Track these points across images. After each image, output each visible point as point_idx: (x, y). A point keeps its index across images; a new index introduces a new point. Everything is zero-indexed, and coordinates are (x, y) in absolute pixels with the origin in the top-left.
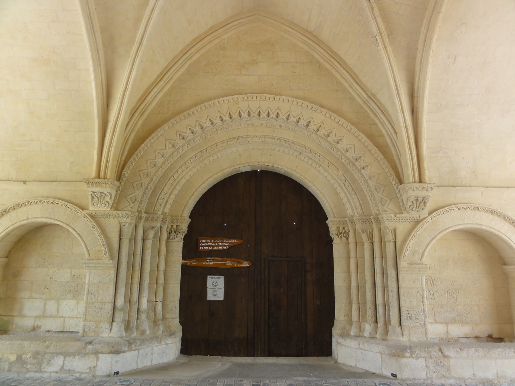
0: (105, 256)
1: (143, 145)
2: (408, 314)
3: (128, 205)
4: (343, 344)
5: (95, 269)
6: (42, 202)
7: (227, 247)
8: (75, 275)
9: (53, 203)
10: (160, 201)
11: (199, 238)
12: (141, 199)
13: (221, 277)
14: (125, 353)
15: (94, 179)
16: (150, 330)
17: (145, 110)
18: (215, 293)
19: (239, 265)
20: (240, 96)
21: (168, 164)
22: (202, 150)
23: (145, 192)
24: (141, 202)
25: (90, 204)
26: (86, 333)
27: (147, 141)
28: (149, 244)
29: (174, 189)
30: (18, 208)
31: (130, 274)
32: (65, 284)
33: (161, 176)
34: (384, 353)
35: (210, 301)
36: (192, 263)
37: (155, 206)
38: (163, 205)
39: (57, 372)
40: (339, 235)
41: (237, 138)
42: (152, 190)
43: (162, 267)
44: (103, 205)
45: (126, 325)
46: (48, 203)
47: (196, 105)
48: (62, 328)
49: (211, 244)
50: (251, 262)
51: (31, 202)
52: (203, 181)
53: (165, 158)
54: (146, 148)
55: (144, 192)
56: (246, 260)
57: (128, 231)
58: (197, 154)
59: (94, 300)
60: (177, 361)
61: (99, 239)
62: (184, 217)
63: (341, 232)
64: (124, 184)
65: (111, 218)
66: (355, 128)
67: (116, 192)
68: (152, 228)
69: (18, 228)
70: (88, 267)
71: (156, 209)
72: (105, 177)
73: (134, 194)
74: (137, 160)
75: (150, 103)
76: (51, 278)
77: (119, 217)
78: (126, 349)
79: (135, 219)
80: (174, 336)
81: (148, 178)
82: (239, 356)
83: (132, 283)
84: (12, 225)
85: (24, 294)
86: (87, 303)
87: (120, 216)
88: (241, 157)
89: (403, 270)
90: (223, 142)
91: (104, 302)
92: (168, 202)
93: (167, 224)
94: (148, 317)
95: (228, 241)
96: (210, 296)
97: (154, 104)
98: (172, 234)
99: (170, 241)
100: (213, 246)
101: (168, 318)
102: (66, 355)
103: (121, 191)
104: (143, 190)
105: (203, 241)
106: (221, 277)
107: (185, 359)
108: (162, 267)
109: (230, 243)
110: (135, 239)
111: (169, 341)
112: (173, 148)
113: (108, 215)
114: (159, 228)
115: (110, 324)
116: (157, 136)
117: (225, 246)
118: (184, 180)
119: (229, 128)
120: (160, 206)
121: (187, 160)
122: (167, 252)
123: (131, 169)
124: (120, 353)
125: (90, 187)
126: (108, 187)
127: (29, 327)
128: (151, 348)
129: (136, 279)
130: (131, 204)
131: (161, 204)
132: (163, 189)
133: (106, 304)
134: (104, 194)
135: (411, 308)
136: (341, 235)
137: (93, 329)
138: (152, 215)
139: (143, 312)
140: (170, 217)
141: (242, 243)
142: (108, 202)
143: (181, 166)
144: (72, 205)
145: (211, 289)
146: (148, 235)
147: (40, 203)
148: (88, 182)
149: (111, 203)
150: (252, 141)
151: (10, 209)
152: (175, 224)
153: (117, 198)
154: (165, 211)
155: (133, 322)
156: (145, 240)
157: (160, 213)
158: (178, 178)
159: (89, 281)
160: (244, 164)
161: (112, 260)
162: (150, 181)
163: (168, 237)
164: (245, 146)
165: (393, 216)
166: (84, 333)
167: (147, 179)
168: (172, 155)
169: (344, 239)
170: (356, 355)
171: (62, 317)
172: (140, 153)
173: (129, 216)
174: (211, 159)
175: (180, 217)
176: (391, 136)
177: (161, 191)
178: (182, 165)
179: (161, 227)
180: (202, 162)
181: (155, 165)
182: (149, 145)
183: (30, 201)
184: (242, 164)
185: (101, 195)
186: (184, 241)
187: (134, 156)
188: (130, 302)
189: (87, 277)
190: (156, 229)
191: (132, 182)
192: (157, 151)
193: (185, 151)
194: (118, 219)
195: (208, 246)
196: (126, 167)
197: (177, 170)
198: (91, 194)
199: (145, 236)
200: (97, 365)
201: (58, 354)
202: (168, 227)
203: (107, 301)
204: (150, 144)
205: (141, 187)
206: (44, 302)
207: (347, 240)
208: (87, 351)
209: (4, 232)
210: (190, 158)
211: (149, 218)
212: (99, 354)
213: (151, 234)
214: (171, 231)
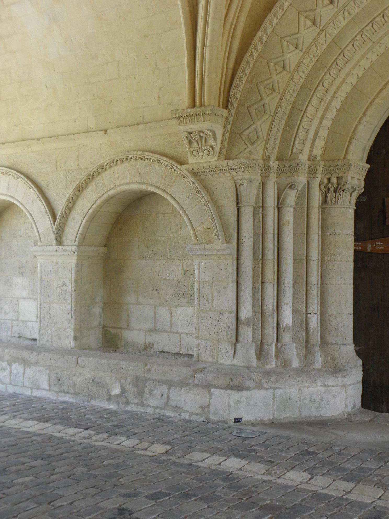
1: (259, 33)
5: (206, 259)
6: (129, 158)
8: (188, 270)
9: (142, 159)
11: (386, 199)
12: (268, 135)
14: (250, 390)
16: (300, 360)
21: (310, 62)
22: (374, 19)
23: (274, 121)
24: (268, 140)
25: (189, 154)
27: (266, 23)
30: (103, 172)
31: (258, 266)
32: (176, 284)
33: (300, 86)
36: (374, 247)
37: (293, 146)
38: (308, 143)
39: (161, 408)
43: (314, 255)
46: (136, 160)
48: (179, 349)
51: (115, 160)
53: (304, 51)
54: (264, 39)
55: (271, 122)
58: (364, 28)
59: (207, 307)
65: (221, 175)
67: (225, 127)
68: (292, 186)
69: (108, 201)
71: (295, 150)
72: (202, 105)
73: (252, 128)
74: (254, 65)
76: (158, 276)
77: (232, 170)
78: (252, 385)
81: (275, 94)
84: (99, 198)
85: (130, 298)
92: (318, 135)
98: (330, 194)
99: (327, 208)
101: (331, 344)
102: (170, 384)
107: (368, 415)
108: (314, 255)
110: (263, 207)
112: (314, 27)
113: (217, 169)
114: (305, 185)
115: (231, 346)
116: (283, 9)
118: (347, 88)
120: (303, 144)
121: (345, 46)
123: (244, 82)
124: (242, 390)
125: (182, 125)
126: (207, 120)
127: (139, 344)
128: (297, 390)
129: (270, 274)
130: (249, 145)
132: (305, 112)
133: (224, 314)
138: (287, 162)
140: (322, 163)
142: (212, 147)
143: (335, 61)
144: (165, 159)
146: (284, 198)
147: (127, 161)
148: (179, 117)
149: (218, 147)
151: (93, 174)
152: (334, 175)
154: (314, 153)
156: (281, 207)
157: (304, 157)
158: (331, 85)
159: (199, 278)
161: (227, 243)
163: (325, 201)
167: (272, 96)
168: (315, 42)
171: (177, 332)
172: (255, 49)
173: (246, 167)
177: (303, 116)
178: (336, 59)
179: (308, 182)
180: (378, 43)
181: (284, 68)
183: (114, 159)
185: (200, 136)
187: (247, 57)
190: (300, 187)
191: (247, 106)
194: (231, 175)
196: (236, 79)
197: (329, 69)
199: (281, 200)
200: (210, 404)
201: (162, 382)
202: (323, 183)
203: (225, 309)
204: (272, 29)
205: (265, 112)
206: (154, 309)
208: (196, 382)
209: (92, 208)
210: (350, 40)
212: (212, 388)
214: (329, 189)
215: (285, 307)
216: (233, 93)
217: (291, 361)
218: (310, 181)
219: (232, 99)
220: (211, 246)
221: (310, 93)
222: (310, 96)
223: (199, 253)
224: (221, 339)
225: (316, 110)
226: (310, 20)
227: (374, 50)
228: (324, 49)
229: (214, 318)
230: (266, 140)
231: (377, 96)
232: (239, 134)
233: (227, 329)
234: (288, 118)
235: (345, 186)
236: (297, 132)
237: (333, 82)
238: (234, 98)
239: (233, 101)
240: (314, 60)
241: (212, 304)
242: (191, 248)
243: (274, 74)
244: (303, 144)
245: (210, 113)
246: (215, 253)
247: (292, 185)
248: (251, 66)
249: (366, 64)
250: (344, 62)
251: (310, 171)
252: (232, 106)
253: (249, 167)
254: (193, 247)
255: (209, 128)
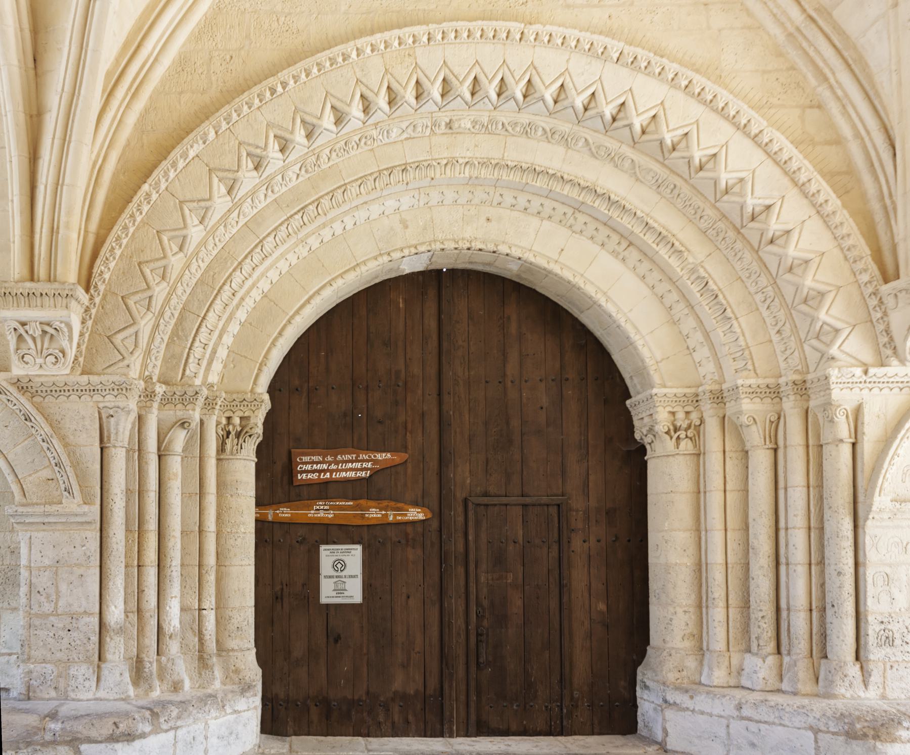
0: (66, 493)
1: (146, 187)
2: (882, 632)
3: (118, 359)
4: (684, 706)
5: (44, 530)
7: (366, 473)
10: (198, 351)
13: (354, 549)
15: (20, 284)
16: (191, 679)
17: (141, 83)
18: (339, 587)
19: (400, 518)
20: (421, 30)
22: (306, 206)
23: (158, 325)
26: (34, 692)
27: (158, 173)
28: (175, 465)
29: (231, 319)
33: (196, 280)
34: (825, 729)
35: (327, 605)
36: (278, 514)
38: (204, 363)
40: (672, 432)
41: (403, 167)
42: (175, 320)
44: (51, 359)
45: (135, 670)
47: (291, 61)
49: (325, 467)
50: (432, 511)
52: (306, 297)
54: (154, 196)
55: (154, 326)
56: (416, 504)
57: (123, 429)
60: (261, 751)
61: (46, 450)
62: (259, 394)
63: (678, 425)
64: (101, 302)
65: (74, 397)
66: (760, 119)
67: (83, 323)
70: (23, 523)
71: (188, 372)
72: (50, 277)
73: (131, 330)
75: (156, 59)
78: (147, 728)
79: (137, 398)
80: (252, 693)
81: (164, 284)
82: (406, 735)
83: (141, 564)
86: (29, 615)
87: (98, 390)
88: (406, 227)
89: (876, 516)
90: (362, 181)
91: (74, 614)
92: (217, 355)
93: (216, 412)
94: (184, 647)
95: (370, 457)
96: (328, 594)
97: (167, 61)
98: (230, 439)
100: (331, 471)
101: (233, 650)
103: (95, 323)
104: (151, 320)
105: (306, 459)
106: (354, 549)
109: (375, 462)
110: (139, 450)
111: (242, 704)
112: (229, 198)
113: (66, 388)
115: (94, 668)
117: (362, 470)
119: (380, 137)
120: (199, 364)
121: (264, 235)
122: (221, 485)
124: (133, 740)
125: (9, 309)
128: (203, 724)
129: (151, 555)
130: (125, 355)
131: (199, 360)
132: (204, 318)
134: (51, 326)
135: (893, 615)
136: (678, 433)
137: (51, 680)
139: (173, 637)
140: (224, 395)
141: (406, 461)
142: (63, 352)
143: (249, 253)
145: (330, 577)
146: (170, 442)
149: (71, 354)
150: (443, 176)
153: (86, 340)
155: (150, 662)
156: (165, 455)
158: (241, 287)
160: (416, 248)
162: (169, 293)
163: (221, 449)
164: (420, 193)
165: (858, 371)
166: (29, 690)
169: (686, 444)
170: (728, 733)
173: (122, 389)
174: (327, 234)
175: (249, 394)
176: (867, 139)
177: (200, 324)
182: (163, 186)
184: (409, 247)
186: (257, 457)
187: (124, 218)
188: (138, 612)
189: (24, 551)
192: (188, 204)
193: (258, 210)
194: (94, 400)
195: (320, 471)
197: (240, 263)
198: (15, 329)
199: (164, 444)
203: (82, 610)
205: (148, 309)
207: (695, 446)
210: (271, 229)
211: (172, 396)
212: (82, 743)
213: (179, 438)
214: (229, 433)
215: (173, 602)
216: (99, 271)
217: (182, 681)
218: (205, 419)
219: (96, 280)
220: (57, 509)
221: (212, 293)
222: (212, 297)
223: (31, 520)
224: (74, 659)
225: (217, 318)
226: (225, 185)
227: (296, 250)
228: (233, 233)
229: (61, 625)
230: (145, 352)
231: (297, 312)
232: (108, 337)
233: (85, 641)
234: (176, 324)
235: (253, 430)
236: (192, 345)
237: (243, 282)
238: (100, 280)
239: (99, 284)
240: (220, 246)
241: (56, 604)
242: (16, 511)
243: (169, 254)
244: (199, 364)
245: (70, 294)
246: (64, 520)
247: (184, 423)
248: (130, 235)
249: (283, 266)
250: (261, 258)
251: (205, 404)
252: (95, 291)
253: (127, 389)
254: (20, 509)
255: (62, 319)
